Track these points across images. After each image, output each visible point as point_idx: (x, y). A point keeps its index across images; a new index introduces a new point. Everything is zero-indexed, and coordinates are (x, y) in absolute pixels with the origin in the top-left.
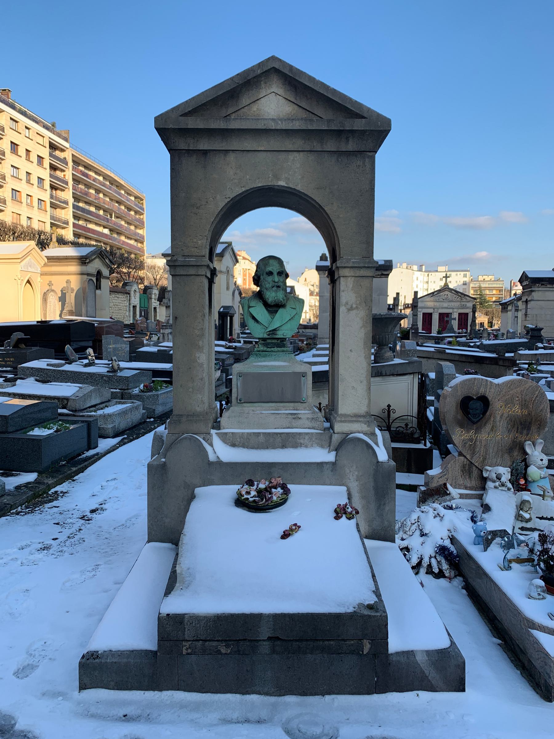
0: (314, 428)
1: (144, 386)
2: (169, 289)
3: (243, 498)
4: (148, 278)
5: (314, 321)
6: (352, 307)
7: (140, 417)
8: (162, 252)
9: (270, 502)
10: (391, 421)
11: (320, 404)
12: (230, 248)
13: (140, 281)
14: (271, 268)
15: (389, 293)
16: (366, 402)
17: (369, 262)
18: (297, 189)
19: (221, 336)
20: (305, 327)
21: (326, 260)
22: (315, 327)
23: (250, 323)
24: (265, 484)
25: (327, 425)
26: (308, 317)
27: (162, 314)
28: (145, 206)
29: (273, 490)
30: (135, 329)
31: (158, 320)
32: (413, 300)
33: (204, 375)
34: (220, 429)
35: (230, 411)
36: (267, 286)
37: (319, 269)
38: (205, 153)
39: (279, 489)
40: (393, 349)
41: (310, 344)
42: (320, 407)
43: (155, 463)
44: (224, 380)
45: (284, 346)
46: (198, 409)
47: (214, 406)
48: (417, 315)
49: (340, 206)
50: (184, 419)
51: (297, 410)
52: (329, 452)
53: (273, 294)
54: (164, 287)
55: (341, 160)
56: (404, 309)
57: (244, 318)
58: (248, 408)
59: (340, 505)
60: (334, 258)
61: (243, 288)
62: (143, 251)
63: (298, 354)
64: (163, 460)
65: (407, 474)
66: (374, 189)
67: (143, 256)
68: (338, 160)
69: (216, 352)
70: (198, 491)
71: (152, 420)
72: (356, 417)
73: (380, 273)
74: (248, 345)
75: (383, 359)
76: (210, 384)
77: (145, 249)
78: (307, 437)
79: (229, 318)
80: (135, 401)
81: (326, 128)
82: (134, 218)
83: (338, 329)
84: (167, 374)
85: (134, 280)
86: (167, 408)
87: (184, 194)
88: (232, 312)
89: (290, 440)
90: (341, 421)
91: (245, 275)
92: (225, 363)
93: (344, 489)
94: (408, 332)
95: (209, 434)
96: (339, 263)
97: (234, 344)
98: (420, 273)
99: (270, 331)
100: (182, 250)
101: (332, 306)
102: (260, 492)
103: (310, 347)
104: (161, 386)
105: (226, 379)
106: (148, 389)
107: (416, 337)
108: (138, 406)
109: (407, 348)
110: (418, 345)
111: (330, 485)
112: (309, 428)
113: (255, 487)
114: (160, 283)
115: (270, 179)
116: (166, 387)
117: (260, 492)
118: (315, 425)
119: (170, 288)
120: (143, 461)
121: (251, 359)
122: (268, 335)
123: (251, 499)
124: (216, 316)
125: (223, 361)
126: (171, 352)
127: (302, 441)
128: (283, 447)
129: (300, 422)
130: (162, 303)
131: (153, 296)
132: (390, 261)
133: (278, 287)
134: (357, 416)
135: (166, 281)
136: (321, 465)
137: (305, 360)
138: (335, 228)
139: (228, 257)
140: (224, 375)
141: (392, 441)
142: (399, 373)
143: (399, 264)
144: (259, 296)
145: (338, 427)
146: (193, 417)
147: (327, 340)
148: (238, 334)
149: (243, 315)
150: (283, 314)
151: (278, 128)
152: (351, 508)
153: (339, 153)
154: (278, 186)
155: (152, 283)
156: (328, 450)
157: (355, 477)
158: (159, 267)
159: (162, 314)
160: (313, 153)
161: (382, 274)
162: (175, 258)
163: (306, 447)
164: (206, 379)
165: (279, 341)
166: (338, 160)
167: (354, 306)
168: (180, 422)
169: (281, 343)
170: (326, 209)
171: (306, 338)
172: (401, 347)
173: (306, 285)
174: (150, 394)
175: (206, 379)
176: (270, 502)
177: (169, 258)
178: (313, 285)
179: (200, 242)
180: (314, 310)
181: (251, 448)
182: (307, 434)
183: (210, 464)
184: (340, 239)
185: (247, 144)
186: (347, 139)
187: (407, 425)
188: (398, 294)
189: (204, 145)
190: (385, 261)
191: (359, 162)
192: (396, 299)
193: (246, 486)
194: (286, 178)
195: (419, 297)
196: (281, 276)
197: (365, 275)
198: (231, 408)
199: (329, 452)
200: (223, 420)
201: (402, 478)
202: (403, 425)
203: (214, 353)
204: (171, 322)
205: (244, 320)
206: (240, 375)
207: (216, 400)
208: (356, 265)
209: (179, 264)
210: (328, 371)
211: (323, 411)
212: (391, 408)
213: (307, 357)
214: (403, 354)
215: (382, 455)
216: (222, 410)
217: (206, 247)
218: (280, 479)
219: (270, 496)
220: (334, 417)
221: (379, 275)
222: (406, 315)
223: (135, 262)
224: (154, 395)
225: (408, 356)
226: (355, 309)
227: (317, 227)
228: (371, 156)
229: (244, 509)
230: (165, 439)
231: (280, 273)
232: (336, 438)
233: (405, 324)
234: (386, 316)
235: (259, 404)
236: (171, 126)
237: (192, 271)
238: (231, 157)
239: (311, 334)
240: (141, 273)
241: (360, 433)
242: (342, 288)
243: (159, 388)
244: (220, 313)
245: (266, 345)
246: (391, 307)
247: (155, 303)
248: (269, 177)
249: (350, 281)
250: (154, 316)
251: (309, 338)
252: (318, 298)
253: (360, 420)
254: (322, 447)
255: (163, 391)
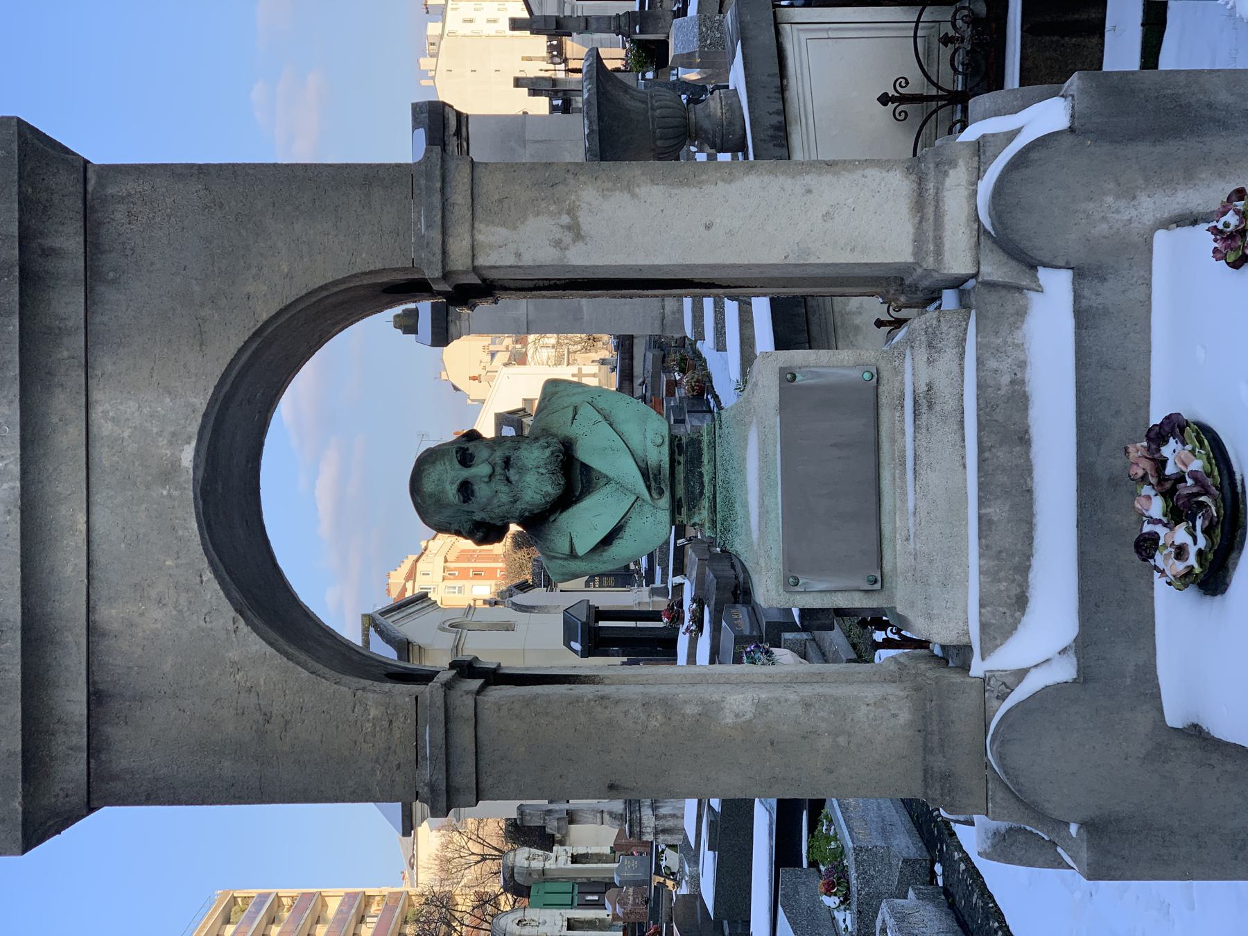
0: (962, 342)
1: (828, 893)
2: (514, 815)
3: (1197, 570)
4: (480, 881)
5: (606, 349)
6: (569, 228)
7: (930, 907)
8: (397, 834)
9: (1210, 481)
10: (934, 92)
11: (879, 323)
12: (381, 619)
13: (489, 908)
14: (448, 487)
15: (516, 110)
16: (872, 172)
17: (429, 177)
18: (205, 406)
19: (659, 647)
20: (626, 377)
21: (414, 314)
22: (625, 345)
23: (621, 551)
24: (1149, 498)
25: (949, 298)
26: (595, 369)
27: (594, 836)
28: (254, 892)
29: (1170, 470)
30: (641, 924)
31: (613, 850)
32: (536, 31)
33: (793, 697)
34: (968, 648)
35: (910, 615)
36: (504, 498)
37: (442, 337)
38: (96, 697)
39: (1166, 451)
40: (696, 92)
41: (683, 359)
42: (890, 323)
43: (1084, 855)
44: (804, 636)
45: (695, 443)
46: (905, 716)
47: (893, 667)
48: (587, 19)
49: (254, 271)
50: (938, 763)
51: (902, 398)
52: (1039, 290)
53: (531, 478)
54: (507, 832)
55: (115, 270)
56: (566, 61)
57: (601, 575)
58: (898, 556)
59: (1216, 250)
60: (416, 287)
61: (505, 577)
62: (396, 897)
63: (716, 397)
64: (1073, 829)
65: (1107, 35)
66: (200, 166)
67: (409, 896)
68: (113, 281)
69: (712, 661)
70: (1174, 718)
71: (938, 868)
72: (925, 207)
73: (454, 141)
74: (687, 561)
75: (730, 123)
76: (822, 679)
77: (386, 890)
78: (992, 364)
79: (601, 624)
80: (879, 924)
81: (16, 321)
82: (291, 927)
83: (641, 268)
84: (787, 813)
85: (485, 926)
86: (899, 819)
87: (227, 764)
88: (585, 612)
89: (1000, 418)
90: (939, 252)
91: (463, 574)
92: (747, 632)
93: (1160, 237)
94: (641, 45)
95: (984, 681)
96: (432, 272)
97: (686, 608)
98: (449, 13)
99: (649, 488)
100: (399, 766)
101: (566, 288)
102: (1178, 513)
103: (691, 361)
104: (828, 839)
105: (805, 629)
106: (837, 881)
107: (657, 18)
108: (893, 912)
109: (694, 46)
110: (682, 12)
111: (1149, 285)
112: (962, 356)
113: (1161, 530)
114: (494, 843)
115: (176, 493)
116: (831, 822)
117: (1178, 513)
118: (949, 333)
119: (510, 809)
120: (1078, 895)
121: (738, 546)
122: (661, 493)
123: (1202, 542)
124: (595, 664)
125: (740, 640)
126: (715, 803)
127: (1005, 379)
128: (1023, 439)
129: (944, 388)
130: (558, 836)
131: (537, 865)
132: (417, 109)
133: (507, 463)
134: (919, 204)
135: (489, 820)
136: (1083, 318)
137: (735, 373)
138: (322, 288)
139: (411, 627)
140: (787, 636)
141: (1000, 85)
142: (777, 71)
143: (424, 83)
144: (537, 523)
145: (958, 262)
146: (930, 730)
147: (670, 304)
148: (654, 592)
149: (592, 578)
150: (597, 448)
151: (16, 469)
152: (1224, 214)
153: (92, 278)
154: (196, 467)
155: (495, 869)
156: (1032, 295)
157: (1122, 203)
158: (445, 847)
159: (594, 836)
160: (91, 360)
161: (458, 133)
162: (424, 791)
163: (1023, 365)
164: (807, 691)
165: (681, 459)
166: (113, 281)
167: (565, 219)
168: (946, 777)
169: (685, 452)
170: (265, 317)
171: (668, 374)
172: (689, 66)
173: (497, 376)
174: (853, 875)
175: (807, 691)
176: (1210, 481)
177: (418, 807)
178: (493, 355)
179: (373, 712)
180: (573, 348)
181: (1031, 544)
182: (980, 362)
183: (1084, 676)
184: (357, 270)
185: (69, 569)
186: (48, 253)
187: (946, 40)
188: (518, 83)
189: (72, 701)
190: (414, 128)
191: (118, 216)
192: (535, 87)
193: (1159, 559)
194: (170, 443)
195: (525, 14)
196: (472, 457)
197: (468, 187)
198: (900, 610)
199: (1039, 290)
200: (940, 634)
201: (1121, 49)
202: (947, 52)
203: (717, 668)
204: (618, 806)
205: (608, 575)
206: (791, 582)
207: (872, 661)
208: (438, 218)
209: (442, 776)
210: (772, 300)
211: (904, 313)
212: (891, 93)
213: (724, 369)
214: (711, 56)
215: (1048, 115)
216: (905, 643)
217: (389, 694)
218: (1131, 449)
219: (1190, 482)
220: (922, 277)
221: (460, 146)
222: (589, 54)
223: (429, 922)
224: (858, 863)
225: (720, 42)
226: (574, 218)
227: (319, 345)
228: (99, 177)
229: (1236, 564)
230: (1003, 825)
231: (466, 459)
232: (995, 268)
233: (615, 55)
234: (595, 119)
235: (885, 519)
236: (17, 805)
237: (464, 736)
238: (108, 614)
239: (650, 356)
240: (464, 903)
241: (975, 193)
242: (510, 260)
243: (833, 845)
244: (587, 652)
245: (693, 500)
246: (559, 102)
247: (558, 860)
248: (170, 496)
249: (490, 234)
250: (600, 861)
251: (662, 364)
252: (531, 338)
253: (932, 191)
254: (1021, 313)
255: (844, 830)
